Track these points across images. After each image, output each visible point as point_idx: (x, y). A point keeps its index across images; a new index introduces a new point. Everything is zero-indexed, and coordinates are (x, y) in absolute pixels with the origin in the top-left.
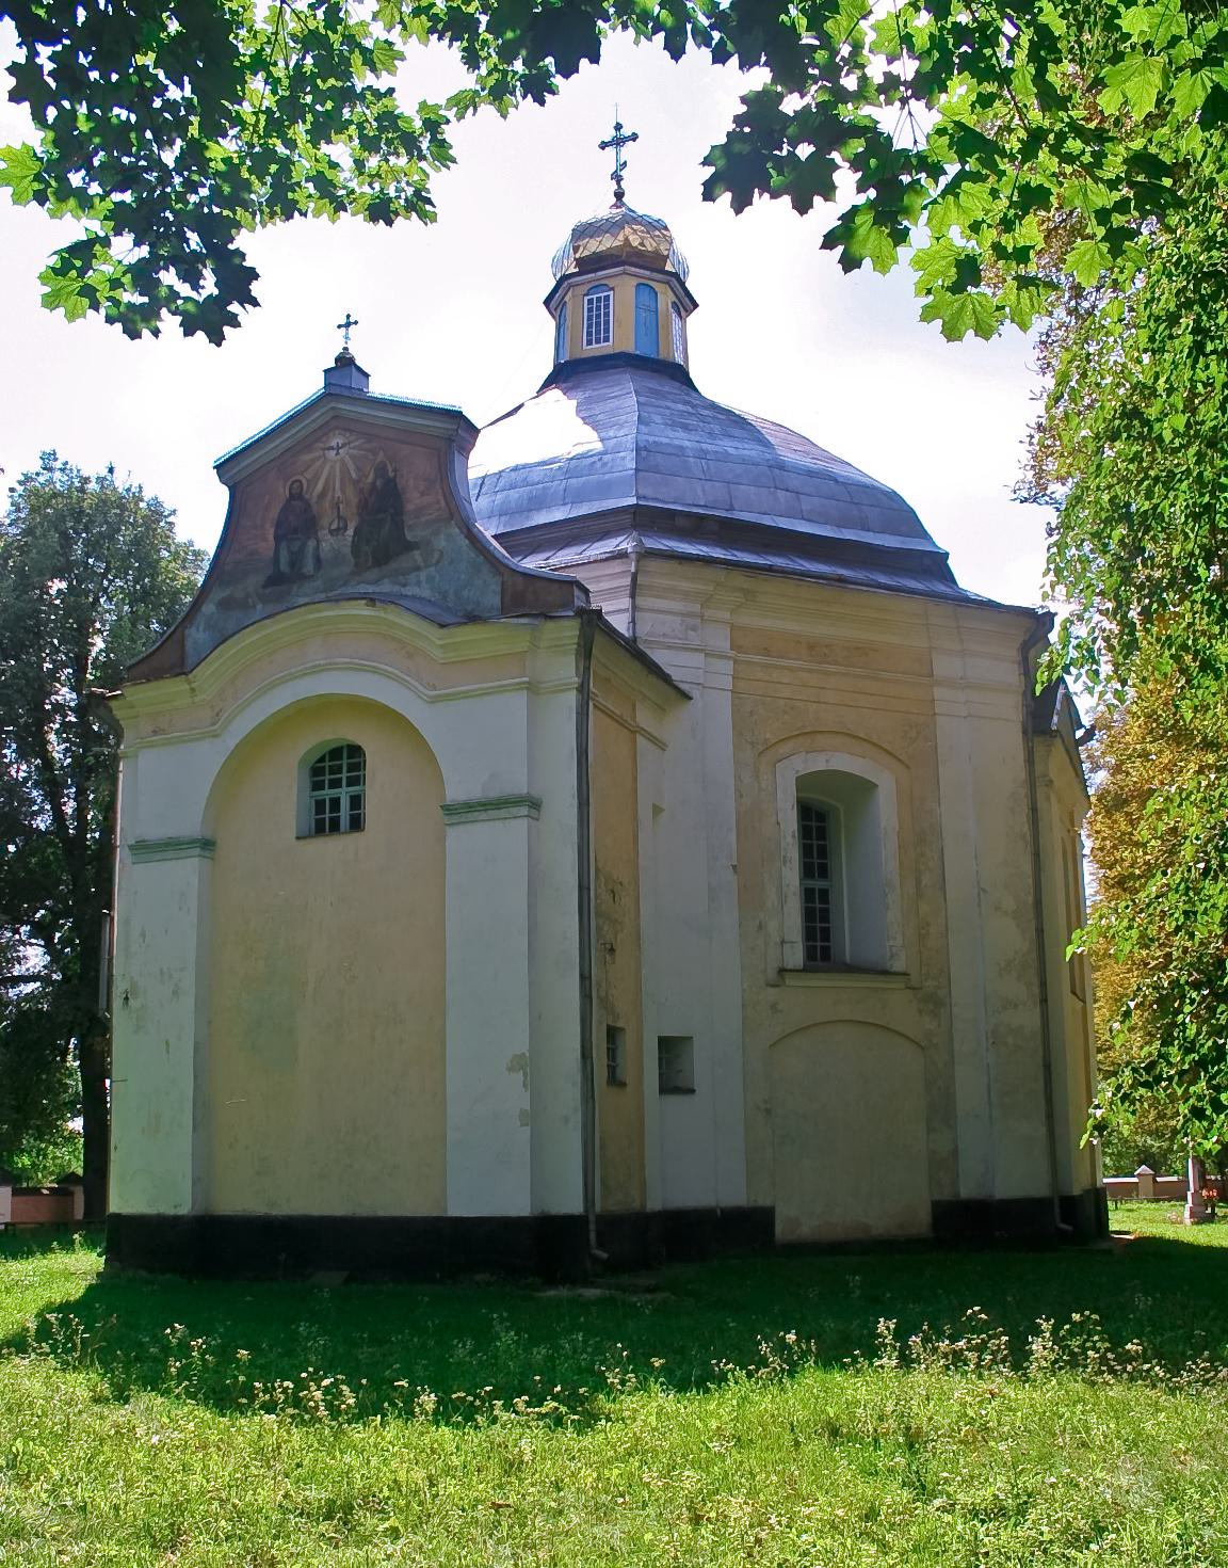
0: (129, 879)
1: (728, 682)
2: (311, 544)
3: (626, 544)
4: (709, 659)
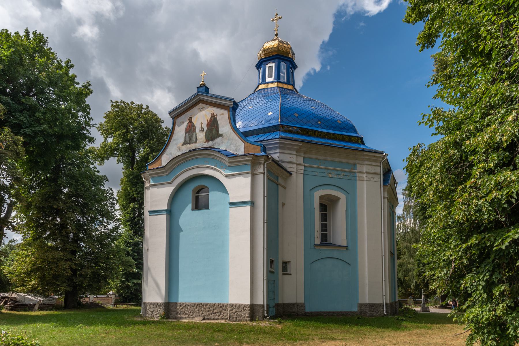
0: (148, 219)
1: (302, 172)
2: (194, 133)
3: (278, 151)
4: (298, 166)
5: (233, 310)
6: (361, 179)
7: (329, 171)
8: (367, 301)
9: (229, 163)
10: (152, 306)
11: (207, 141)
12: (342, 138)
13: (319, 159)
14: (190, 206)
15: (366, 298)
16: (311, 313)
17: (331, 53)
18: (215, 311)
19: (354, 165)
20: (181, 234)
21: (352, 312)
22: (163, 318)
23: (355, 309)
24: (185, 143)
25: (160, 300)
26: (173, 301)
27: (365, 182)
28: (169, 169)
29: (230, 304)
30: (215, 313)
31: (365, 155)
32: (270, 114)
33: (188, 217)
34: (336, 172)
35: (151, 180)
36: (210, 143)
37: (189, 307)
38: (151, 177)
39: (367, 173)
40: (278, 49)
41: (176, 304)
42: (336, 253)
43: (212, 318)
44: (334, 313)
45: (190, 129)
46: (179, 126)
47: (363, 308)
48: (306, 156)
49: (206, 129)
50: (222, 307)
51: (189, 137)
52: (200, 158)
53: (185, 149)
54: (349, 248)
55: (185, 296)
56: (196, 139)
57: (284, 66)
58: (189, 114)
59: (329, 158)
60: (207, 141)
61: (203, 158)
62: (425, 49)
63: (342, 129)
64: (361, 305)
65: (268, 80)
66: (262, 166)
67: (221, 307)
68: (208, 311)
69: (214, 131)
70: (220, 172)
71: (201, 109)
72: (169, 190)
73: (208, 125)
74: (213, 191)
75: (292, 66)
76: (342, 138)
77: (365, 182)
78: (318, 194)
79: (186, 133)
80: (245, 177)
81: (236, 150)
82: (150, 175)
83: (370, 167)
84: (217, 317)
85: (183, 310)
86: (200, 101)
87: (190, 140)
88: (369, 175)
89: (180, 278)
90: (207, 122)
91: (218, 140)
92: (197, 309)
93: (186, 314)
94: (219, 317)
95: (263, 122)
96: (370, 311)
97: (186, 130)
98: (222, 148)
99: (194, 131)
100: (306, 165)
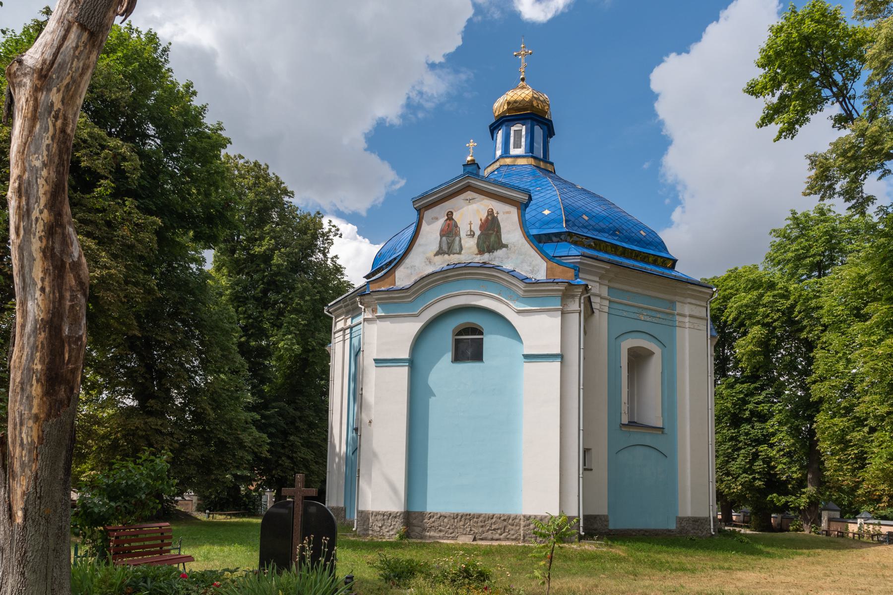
1: (606, 309)
2: (457, 238)
5: (529, 525)
6: (681, 325)
7: (640, 310)
8: (689, 514)
9: (525, 291)
10: (379, 517)
11: (481, 252)
12: (644, 258)
13: (627, 291)
14: (449, 356)
15: (687, 509)
16: (617, 530)
17: (463, 77)
18: (493, 527)
19: (673, 303)
20: (432, 400)
21: (669, 531)
22: (401, 537)
23: (673, 526)
24: (440, 252)
25: (396, 506)
26: (417, 508)
27: (687, 331)
28: (414, 293)
29: (524, 516)
30: (494, 530)
31: (689, 289)
32: (547, 212)
33: (445, 372)
34: (650, 313)
35: (379, 308)
36: (486, 257)
37: (446, 520)
38: (379, 304)
39: (691, 316)
40: (532, 106)
41: (422, 515)
42: (648, 439)
43: (490, 537)
44: (646, 531)
45: (450, 231)
46: (429, 224)
47: (684, 524)
48: (612, 285)
49: (478, 233)
50: (506, 522)
51: (448, 243)
52: (472, 279)
53: (441, 263)
54: (666, 431)
55: (438, 501)
56: (461, 248)
57: (538, 131)
58: (447, 206)
59: (640, 291)
60: (481, 252)
61: (478, 279)
62: (782, 139)
63: (647, 244)
64: (680, 520)
65: (514, 152)
66: (577, 300)
67: (504, 520)
68: (482, 527)
69: (493, 239)
70: (508, 305)
71: (469, 201)
72: (413, 327)
73: (481, 227)
74: (491, 334)
75: (549, 131)
76: (644, 258)
77: (687, 331)
78: (628, 343)
79: (441, 236)
80: (551, 316)
81: (532, 272)
82: (377, 299)
83: (693, 307)
84: (497, 536)
85: (436, 524)
86: (468, 188)
87: (449, 248)
88: (693, 320)
89: (429, 472)
90: (480, 222)
91: (500, 253)
92: (462, 523)
93: (440, 531)
94: (501, 537)
95: (537, 225)
96: (693, 529)
97: (442, 231)
98: (508, 266)
99: (457, 234)
100: (612, 299)
